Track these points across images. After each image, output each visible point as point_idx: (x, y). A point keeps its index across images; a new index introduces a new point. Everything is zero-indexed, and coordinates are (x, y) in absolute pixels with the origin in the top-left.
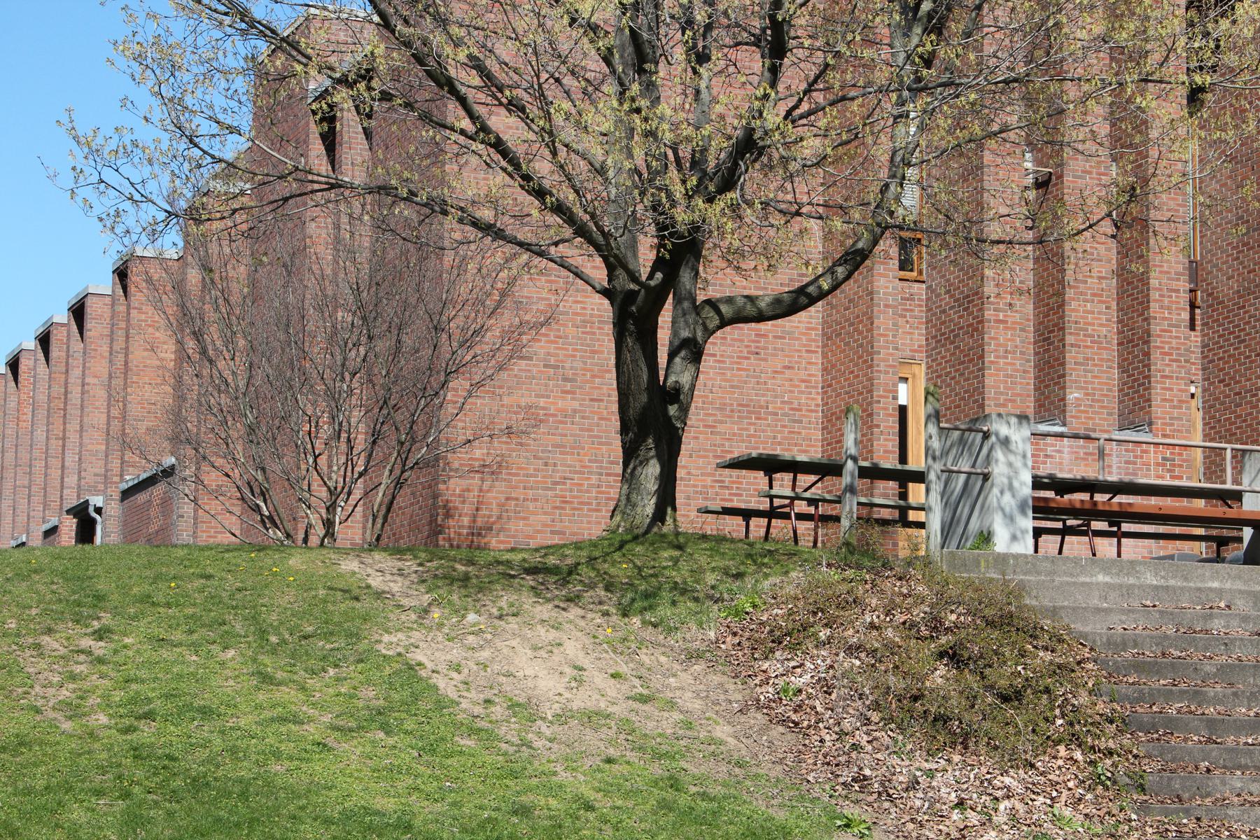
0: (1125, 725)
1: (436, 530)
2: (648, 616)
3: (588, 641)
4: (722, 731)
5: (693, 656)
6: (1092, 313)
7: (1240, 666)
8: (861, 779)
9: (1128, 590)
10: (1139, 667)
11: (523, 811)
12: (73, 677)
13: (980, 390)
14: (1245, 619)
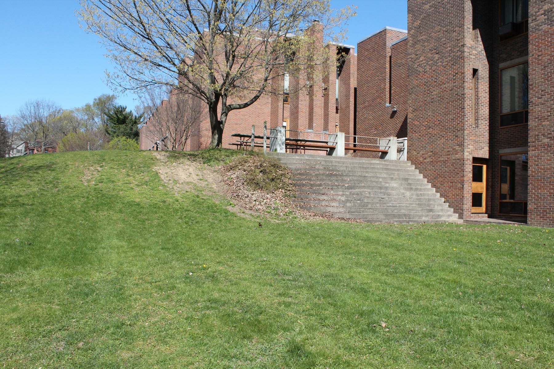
0: (295, 185)
1: (199, 147)
2: (209, 164)
3: (195, 168)
4: (214, 186)
5: (215, 171)
6: (319, 111)
7: (320, 174)
8: (238, 196)
9: (301, 160)
10: (300, 174)
11: (164, 202)
12: (92, 174)
13: (297, 123)
14: (323, 165)
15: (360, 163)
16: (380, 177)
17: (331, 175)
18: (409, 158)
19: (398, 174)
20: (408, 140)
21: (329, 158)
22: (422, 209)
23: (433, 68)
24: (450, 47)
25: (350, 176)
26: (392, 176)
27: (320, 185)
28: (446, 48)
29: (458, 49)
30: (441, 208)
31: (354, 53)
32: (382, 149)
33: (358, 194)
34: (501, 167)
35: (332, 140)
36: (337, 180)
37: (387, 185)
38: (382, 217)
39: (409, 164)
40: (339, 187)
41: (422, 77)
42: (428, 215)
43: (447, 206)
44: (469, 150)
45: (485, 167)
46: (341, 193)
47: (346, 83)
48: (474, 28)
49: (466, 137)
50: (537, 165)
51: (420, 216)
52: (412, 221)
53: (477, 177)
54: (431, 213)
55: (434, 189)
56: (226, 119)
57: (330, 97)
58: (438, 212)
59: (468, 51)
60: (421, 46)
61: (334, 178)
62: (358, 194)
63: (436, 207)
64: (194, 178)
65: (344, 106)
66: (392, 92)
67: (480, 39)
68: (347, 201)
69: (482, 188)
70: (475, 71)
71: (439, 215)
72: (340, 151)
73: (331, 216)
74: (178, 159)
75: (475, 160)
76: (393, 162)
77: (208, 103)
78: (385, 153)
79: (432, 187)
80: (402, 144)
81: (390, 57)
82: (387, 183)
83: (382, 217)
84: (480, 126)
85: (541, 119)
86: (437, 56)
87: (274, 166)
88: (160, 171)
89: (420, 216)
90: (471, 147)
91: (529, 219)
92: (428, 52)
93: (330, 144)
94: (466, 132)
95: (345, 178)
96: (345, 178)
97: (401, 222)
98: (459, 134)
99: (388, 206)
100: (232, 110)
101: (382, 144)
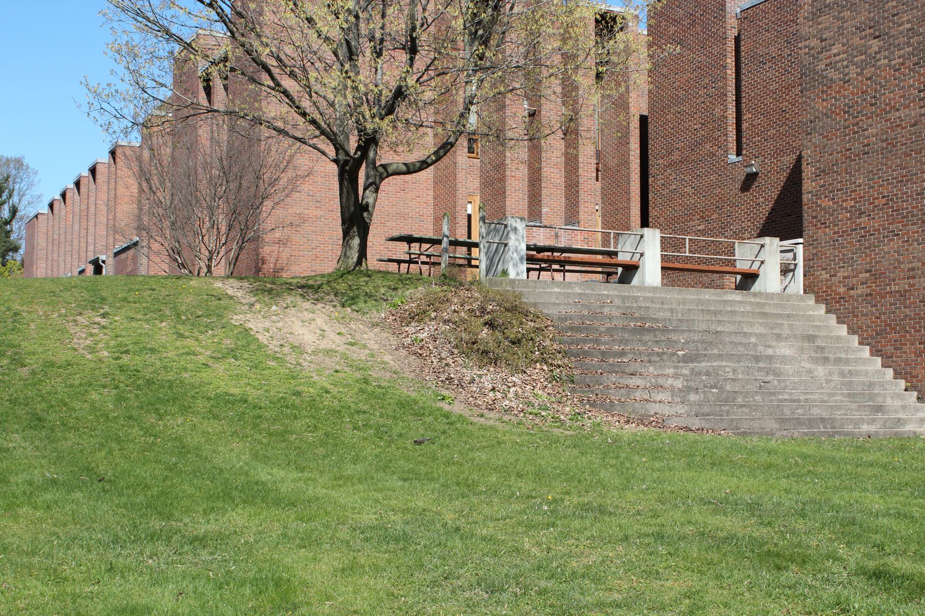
0: (566, 354)
1: (258, 270)
2: (354, 307)
3: (327, 318)
4: (387, 358)
5: (375, 325)
7: (616, 328)
8: (450, 379)
10: (572, 329)
11: (298, 394)
12: (92, 335)
14: (618, 307)
15: (699, 302)
16: (750, 334)
17: (641, 330)
18: (808, 288)
19: (791, 327)
22: (860, 406)
23: (868, 72)
24: (908, 21)
25: (684, 331)
26: (777, 331)
27: (622, 354)
28: (900, 25)
30: (900, 403)
31: (637, 32)
32: (742, 266)
33: (708, 374)
36: (657, 342)
37: (770, 352)
38: (771, 425)
40: (665, 357)
41: (838, 92)
42: (873, 421)
43: (915, 399)
51: (857, 423)
52: (840, 433)
54: (880, 415)
56: (375, 200)
58: (896, 411)
61: (647, 337)
62: (708, 374)
64: (333, 341)
66: (745, 126)
68: (688, 389)
71: (899, 420)
73: (661, 423)
74: (278, 295)
76: (773, 299)
77: (336, 161)
79: (872, 354)
80: (791, 255)
81: (737, 40)
82: (769, 346)
83: (771, 425)
86: (875, 44)
87: (513, 309)
88: (250, 325)
89: (857, 423)
92: (853, 34)
95: (674, 337)
96: (674, 337)
99: (780, 401)
100: (388, 176)
101: (744, 254)
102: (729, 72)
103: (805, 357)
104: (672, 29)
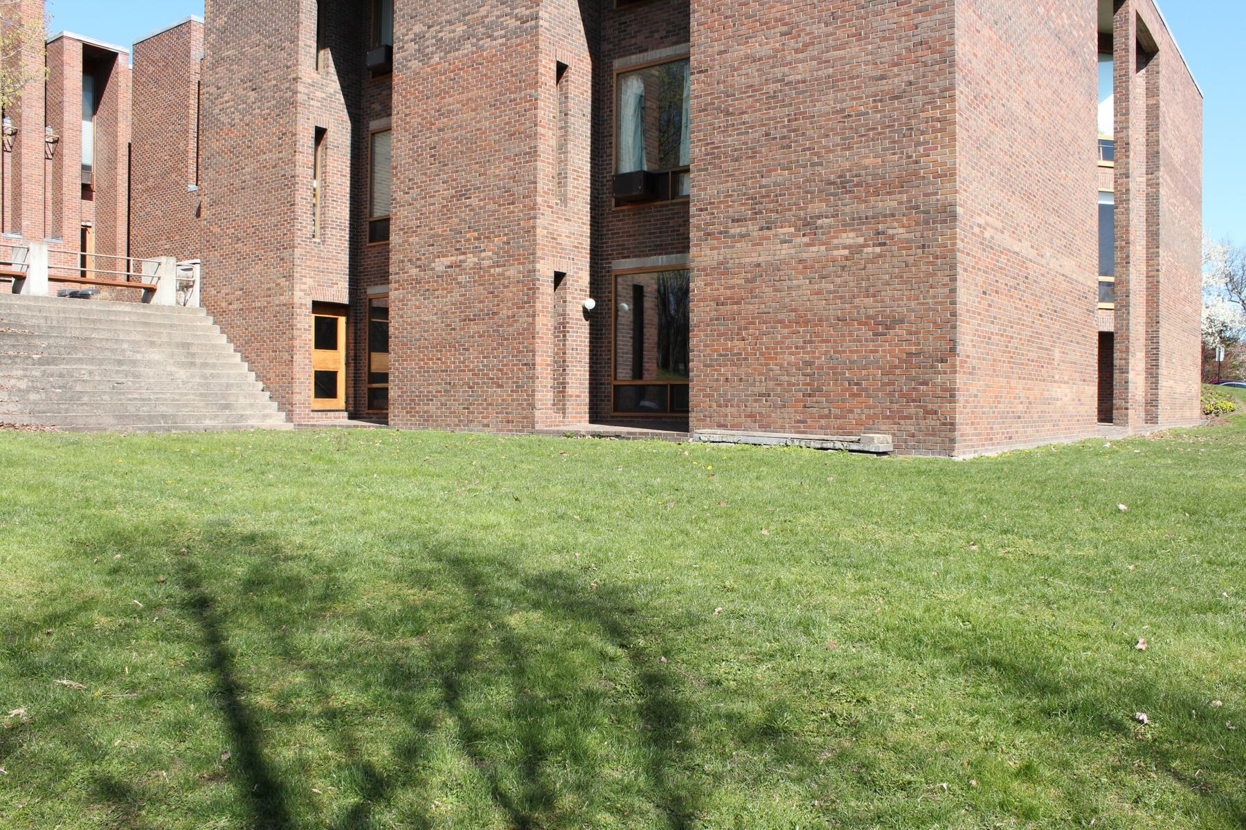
15: (81, 311)
18: (203, 302)
20: (203, 265)
21: (15, 300)
23: (247, 118)
29: (287, 85)
32: (146, 282)
33: (61, 376)
34: (370, 322)
35: (19, 260)
37: (139, 356)
38: (109, 420)
39: (203, 313)
40: (18, 360)
42: (216, 417)
44: (303, 287)
45: (342, 321)
46: (20, 373)
47: (108, 132)
48: (321, 45)
49: (297, 262)
50: (402, 317)
52: (176, 428)
53: (325, 339)
55: (246, 364)
57: (67, 161)
59: (306, 91)
60: (228, 69)
62: (61, 376)
63: (242, 400)
65: (104, 185)
67: (332, 69)
69: (336, 361)
70: (320, 133)
72: (38, 284)
75: (318, 306)
78: (150, 291)
80: (190, 273)
84: (329, 241)
85: (406, 231)
89: (199, 419)
90: (309, 281)
91: (391, 416)
93: (15, 269)
94: (298, 252)
96: (37, 342)
97: (151, 431)
98: (286, 254)
102: (191, 112)
103: (171, 361)
104: (151, 69)
